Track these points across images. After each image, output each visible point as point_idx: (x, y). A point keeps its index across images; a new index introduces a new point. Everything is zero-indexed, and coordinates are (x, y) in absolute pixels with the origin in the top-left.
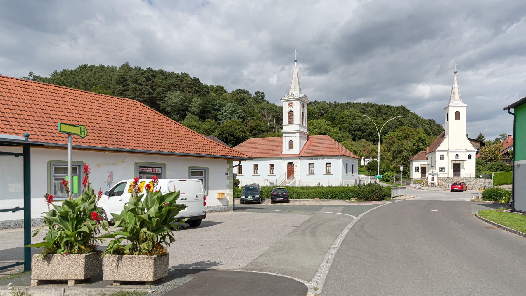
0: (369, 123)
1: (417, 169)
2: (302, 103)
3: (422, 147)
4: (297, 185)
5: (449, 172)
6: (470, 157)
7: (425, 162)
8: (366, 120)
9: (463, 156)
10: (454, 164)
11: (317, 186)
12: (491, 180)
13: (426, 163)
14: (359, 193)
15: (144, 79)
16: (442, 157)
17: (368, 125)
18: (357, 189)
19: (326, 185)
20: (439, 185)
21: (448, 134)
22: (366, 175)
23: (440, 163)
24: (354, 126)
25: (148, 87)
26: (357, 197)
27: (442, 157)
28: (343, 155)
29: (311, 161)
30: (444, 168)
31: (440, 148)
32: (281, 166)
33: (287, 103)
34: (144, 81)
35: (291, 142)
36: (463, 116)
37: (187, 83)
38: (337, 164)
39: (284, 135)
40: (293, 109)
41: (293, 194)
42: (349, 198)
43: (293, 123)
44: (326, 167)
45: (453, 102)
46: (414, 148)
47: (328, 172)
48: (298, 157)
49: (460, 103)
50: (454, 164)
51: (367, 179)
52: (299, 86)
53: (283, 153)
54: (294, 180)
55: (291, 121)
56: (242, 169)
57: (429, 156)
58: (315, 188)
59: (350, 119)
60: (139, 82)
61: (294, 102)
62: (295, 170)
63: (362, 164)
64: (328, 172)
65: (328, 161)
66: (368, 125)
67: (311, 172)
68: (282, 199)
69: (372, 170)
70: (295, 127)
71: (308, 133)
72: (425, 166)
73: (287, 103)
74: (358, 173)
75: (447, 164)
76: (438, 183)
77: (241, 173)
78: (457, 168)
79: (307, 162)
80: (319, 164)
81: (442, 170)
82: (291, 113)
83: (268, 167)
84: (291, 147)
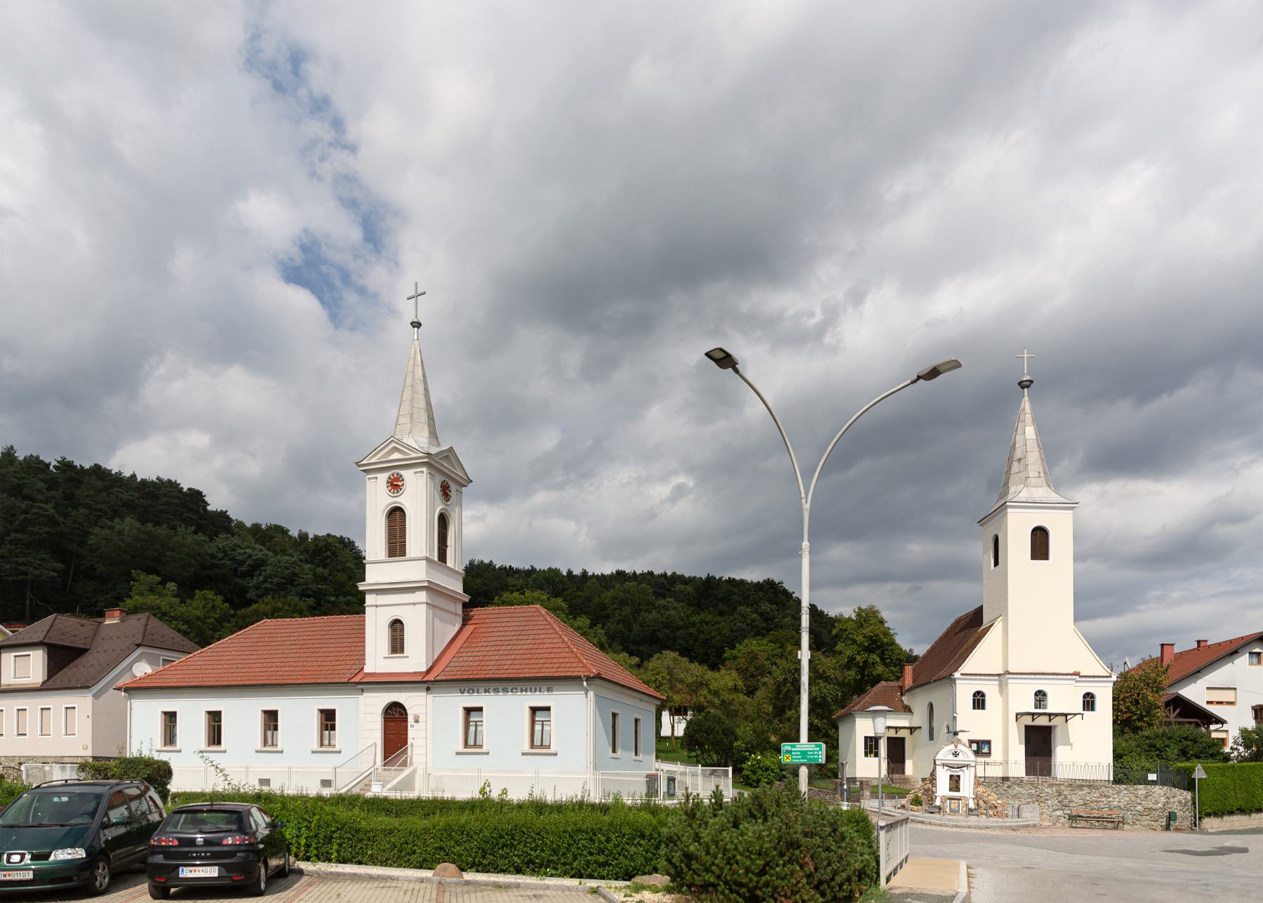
0: (681, 623)
1: (871, 746)
2: (439, 479)
3: (880, 669)
4: (422, 790)
5: (1011, 757)
6: (1089, 702)
7: (902, 721)
8: (672, 612)
9: (1063, 698)
10: (1027, 727)
11: (477, 796)
12: (1188, 795)
13: (906, 723)
14: (689, 857)
15: (41, 485)
16: (979, 701)
17: (679, 628)
18: (673, 826)
19: (517, 794)
20: (982, 807)
21: (1003, 611)
22: (684, 762)
23: (971, 724)
24: (636, 628)
25: (50, 505)
26: (677, 875)
27: (979, 701)
28: (598, 676)
29: (472, 700)
30: (988, 743)
31: (969, 665)
32: (362, 716)
33: (383, 477)
34: (39, 491)
35: (397, 625)
36: (1060, 544)
37: (165, 504)
38: (574, 711)
39: (370, 599)
40: (404, 500)
41: (329, 839)
42: (628, 876)
43: (403, 553)
44: (533, 722)
45: (1018, 492)
46: (852, 674)
47: (538, 744)
48: (426, 682)
49: (1042, 492)
50: (1027, 727)
51: (684, 774)
52: (431, 419)
53: (367, 669)
54: (407, 771)
55: (396, 547)
56: (219, 727)
57: (919, 702)
58: (470, 806)
59: (627, 610)
60: (26, 491)
61: (407, 474)
62: (414, 733)
63: (666, 731)
64: (538, 744)
65: (539, 699)
66: (679, 628)
67: (471, 742)
68: (212, 872)
69: (701, 746)
70: (412, 570)
71: (467, 598)
72: (901, 734)
73: (383, 477)
74: (657, 757)
75: (1000, 727)
76: (977, 797)
77: (219, 743)
78: (1039, 742)
79: (460, 700)
80: (505, 712)
81: (981, 747)
82: (396, 516)
83: (315, 721)
84: (397, 645)
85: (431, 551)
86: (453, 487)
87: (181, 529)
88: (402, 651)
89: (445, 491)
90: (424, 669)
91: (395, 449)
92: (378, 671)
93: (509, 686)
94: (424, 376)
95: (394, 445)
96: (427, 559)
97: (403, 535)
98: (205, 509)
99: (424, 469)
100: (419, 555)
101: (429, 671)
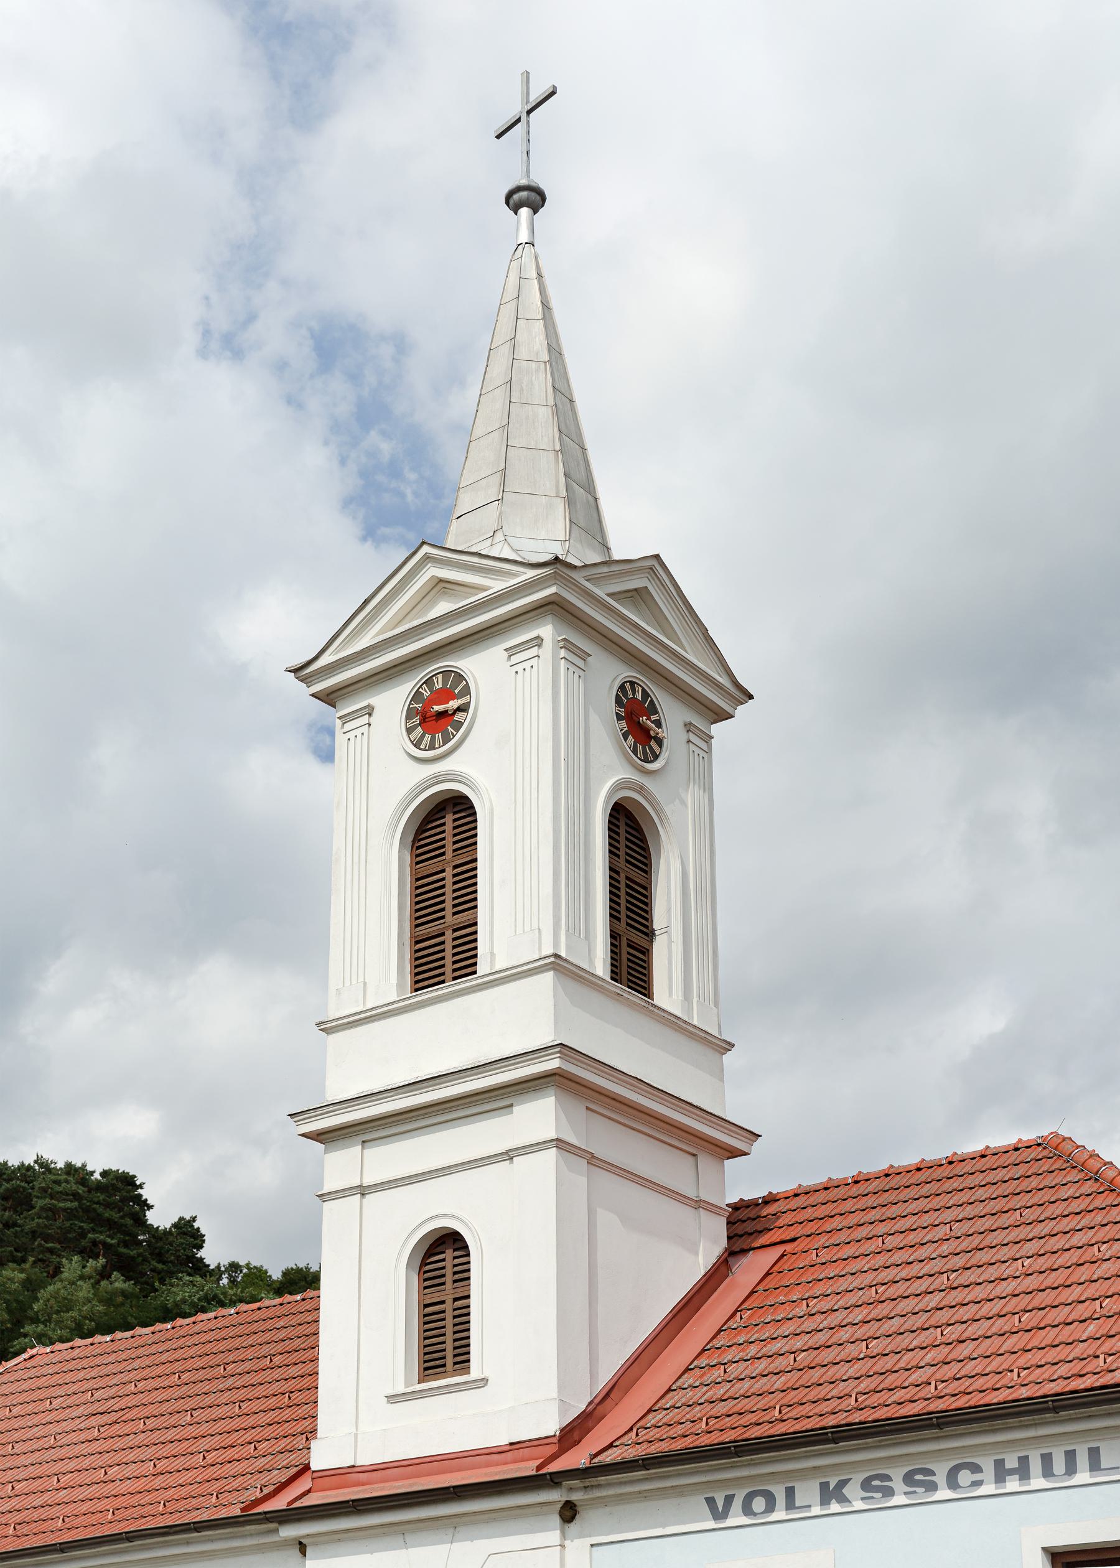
2: (611, 673)
40: (474, 764)
43: (466, 965)
61: (481, 668)
73: (392, 703)
82: (443, 829)
84: (443, 1345)
85: (580, 932)
86: (673, 717)
87: (71, 1266)
88: (463, 1361)
89: (638, 724)
90: (550, 1425)
91: (441, 586)
92: (366, 1459)
93: (937, 1454)
94: (546, 306)
95: (426, 549)
96: (557, 964)
97: (467, 900)
98: (140, 1221)
99: (546, 630)
100: (527, 954)
101: (572, 1434)
